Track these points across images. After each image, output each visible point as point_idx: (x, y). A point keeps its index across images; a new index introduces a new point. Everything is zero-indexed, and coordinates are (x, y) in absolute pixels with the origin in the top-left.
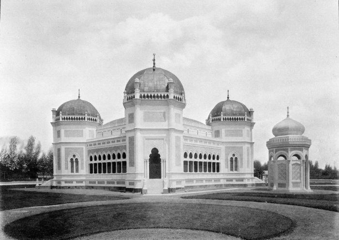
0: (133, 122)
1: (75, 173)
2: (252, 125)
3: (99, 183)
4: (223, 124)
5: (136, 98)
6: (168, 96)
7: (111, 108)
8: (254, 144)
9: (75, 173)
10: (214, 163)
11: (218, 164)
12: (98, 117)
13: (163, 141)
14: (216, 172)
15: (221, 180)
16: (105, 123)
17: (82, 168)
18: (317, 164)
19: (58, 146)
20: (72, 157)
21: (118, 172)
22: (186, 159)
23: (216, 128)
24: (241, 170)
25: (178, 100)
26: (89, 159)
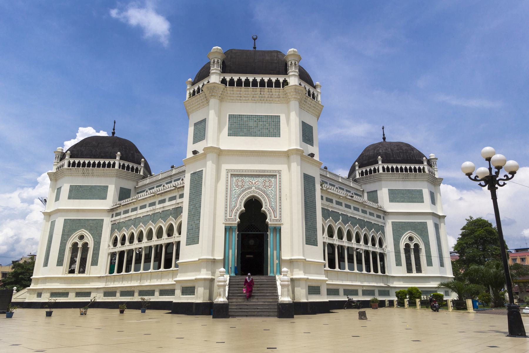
1: (76, 275)
6: (285, 83)
9: (414, 274)
11: (382, 256)
12: (142, 165)
15: (93, 295)
17: (95, 262)
20: (77, 240)
23: (370, 187)
25: (309, 95)
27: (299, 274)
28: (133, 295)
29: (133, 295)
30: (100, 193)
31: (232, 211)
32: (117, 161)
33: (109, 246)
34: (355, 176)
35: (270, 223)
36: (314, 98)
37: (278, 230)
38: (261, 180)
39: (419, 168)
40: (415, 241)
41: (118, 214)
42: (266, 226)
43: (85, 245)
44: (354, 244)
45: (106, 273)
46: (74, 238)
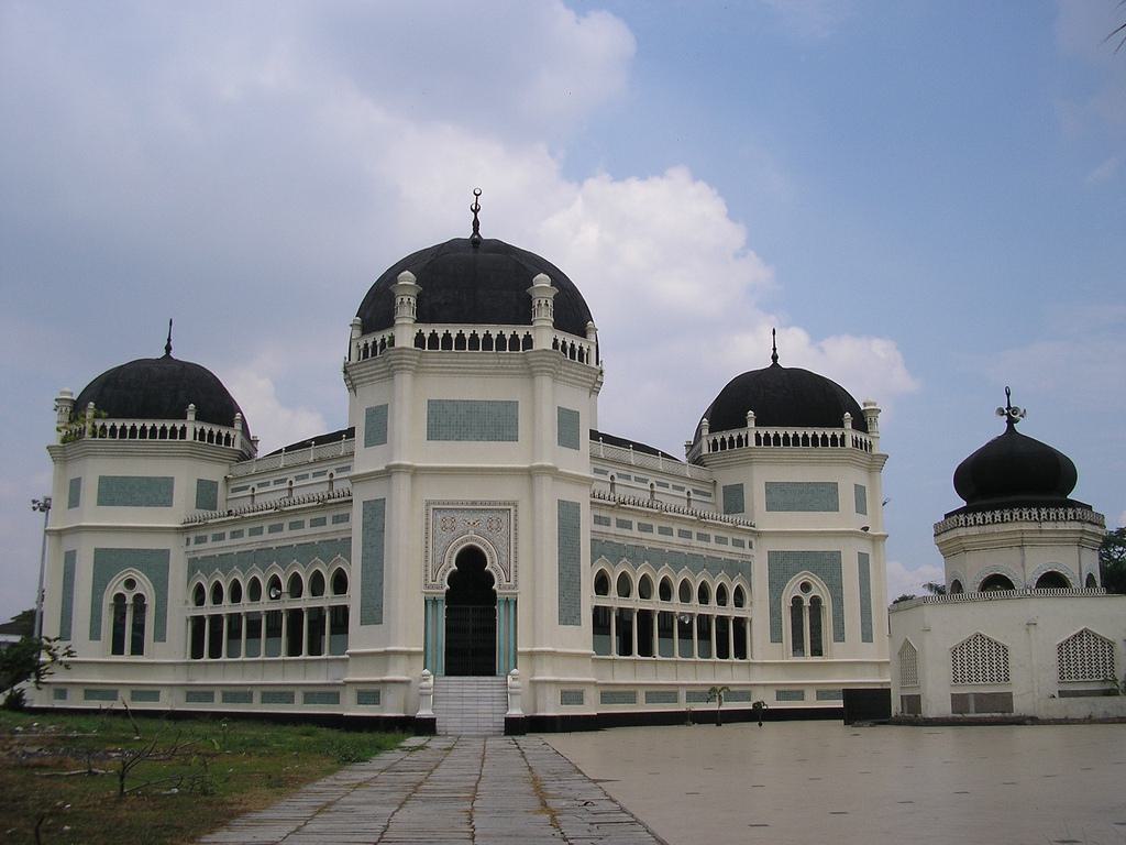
0: (384, 441)
1: (127, 657)
2: (876, 463)
3: (606, 697)
4: (191, 456)
5: (398, 344)
6: (528, 342)
7: (286, 392)
8: (933, 533)
9: (809, 658)
10: (722, 621)
11: (740, 624)
13: (504, 518)
14: (732, 658)
16: (263, 450)
17: (160, 636)
18: (760, 725)
19: (69, 543)
20: (121, 589)
21: (311, 653)
22: (603, 602)
23: (727, 478)
24: (834, 652)
25: (573, 357)
26: (190, 597)
27: (546, 674)
28: (250, 701)
29: (250, 701)
30: (157, 492)
31: (436, 571)
33: (186, 602)
34: (700, 450)
35: (498, 591)
36: (581, 359)
37: (512, 603)
38: (484, 517)
39: (834, 436)
40: (814, 592)
41: (199, 540)
42: (491, 597)
43: (139, 598)
44: (675, 606)
45: (185, 657)
46: (116, 586)
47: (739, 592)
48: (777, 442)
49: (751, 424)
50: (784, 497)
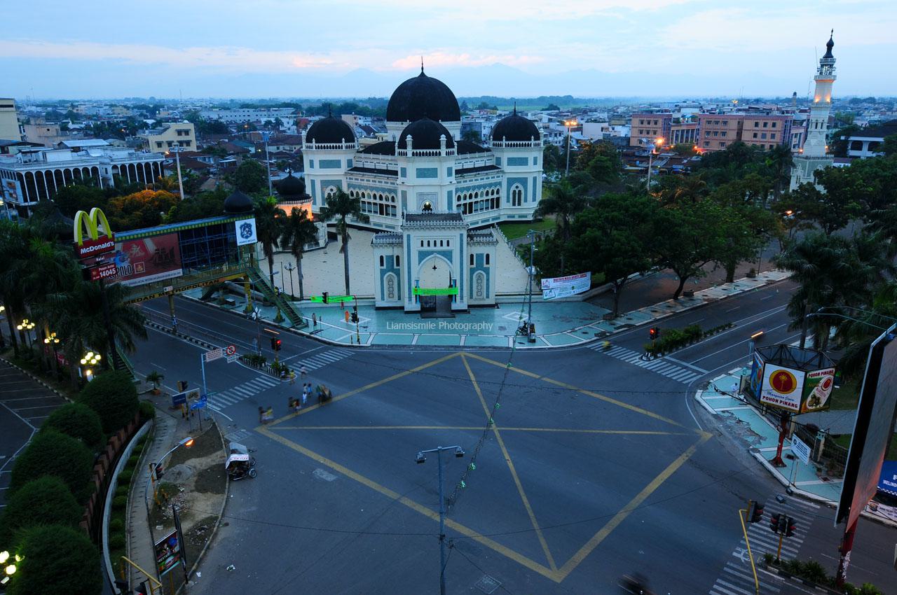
6: (354, 147)
21: (497, 208)
24: (524, 205)
30: (336, 164)
32: (344, 144)
46: (513, 188)
47: (393, 198)
48: (520, 146)
49: (504, 140)
50: (512, 162)
